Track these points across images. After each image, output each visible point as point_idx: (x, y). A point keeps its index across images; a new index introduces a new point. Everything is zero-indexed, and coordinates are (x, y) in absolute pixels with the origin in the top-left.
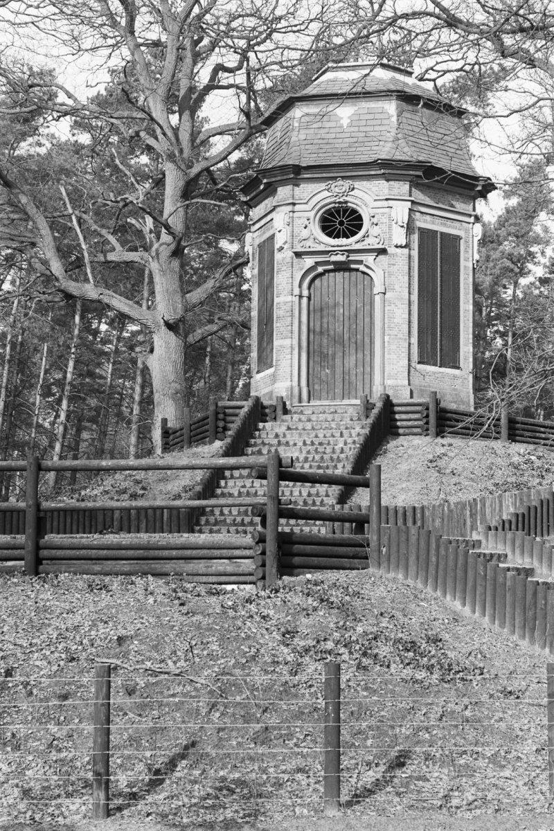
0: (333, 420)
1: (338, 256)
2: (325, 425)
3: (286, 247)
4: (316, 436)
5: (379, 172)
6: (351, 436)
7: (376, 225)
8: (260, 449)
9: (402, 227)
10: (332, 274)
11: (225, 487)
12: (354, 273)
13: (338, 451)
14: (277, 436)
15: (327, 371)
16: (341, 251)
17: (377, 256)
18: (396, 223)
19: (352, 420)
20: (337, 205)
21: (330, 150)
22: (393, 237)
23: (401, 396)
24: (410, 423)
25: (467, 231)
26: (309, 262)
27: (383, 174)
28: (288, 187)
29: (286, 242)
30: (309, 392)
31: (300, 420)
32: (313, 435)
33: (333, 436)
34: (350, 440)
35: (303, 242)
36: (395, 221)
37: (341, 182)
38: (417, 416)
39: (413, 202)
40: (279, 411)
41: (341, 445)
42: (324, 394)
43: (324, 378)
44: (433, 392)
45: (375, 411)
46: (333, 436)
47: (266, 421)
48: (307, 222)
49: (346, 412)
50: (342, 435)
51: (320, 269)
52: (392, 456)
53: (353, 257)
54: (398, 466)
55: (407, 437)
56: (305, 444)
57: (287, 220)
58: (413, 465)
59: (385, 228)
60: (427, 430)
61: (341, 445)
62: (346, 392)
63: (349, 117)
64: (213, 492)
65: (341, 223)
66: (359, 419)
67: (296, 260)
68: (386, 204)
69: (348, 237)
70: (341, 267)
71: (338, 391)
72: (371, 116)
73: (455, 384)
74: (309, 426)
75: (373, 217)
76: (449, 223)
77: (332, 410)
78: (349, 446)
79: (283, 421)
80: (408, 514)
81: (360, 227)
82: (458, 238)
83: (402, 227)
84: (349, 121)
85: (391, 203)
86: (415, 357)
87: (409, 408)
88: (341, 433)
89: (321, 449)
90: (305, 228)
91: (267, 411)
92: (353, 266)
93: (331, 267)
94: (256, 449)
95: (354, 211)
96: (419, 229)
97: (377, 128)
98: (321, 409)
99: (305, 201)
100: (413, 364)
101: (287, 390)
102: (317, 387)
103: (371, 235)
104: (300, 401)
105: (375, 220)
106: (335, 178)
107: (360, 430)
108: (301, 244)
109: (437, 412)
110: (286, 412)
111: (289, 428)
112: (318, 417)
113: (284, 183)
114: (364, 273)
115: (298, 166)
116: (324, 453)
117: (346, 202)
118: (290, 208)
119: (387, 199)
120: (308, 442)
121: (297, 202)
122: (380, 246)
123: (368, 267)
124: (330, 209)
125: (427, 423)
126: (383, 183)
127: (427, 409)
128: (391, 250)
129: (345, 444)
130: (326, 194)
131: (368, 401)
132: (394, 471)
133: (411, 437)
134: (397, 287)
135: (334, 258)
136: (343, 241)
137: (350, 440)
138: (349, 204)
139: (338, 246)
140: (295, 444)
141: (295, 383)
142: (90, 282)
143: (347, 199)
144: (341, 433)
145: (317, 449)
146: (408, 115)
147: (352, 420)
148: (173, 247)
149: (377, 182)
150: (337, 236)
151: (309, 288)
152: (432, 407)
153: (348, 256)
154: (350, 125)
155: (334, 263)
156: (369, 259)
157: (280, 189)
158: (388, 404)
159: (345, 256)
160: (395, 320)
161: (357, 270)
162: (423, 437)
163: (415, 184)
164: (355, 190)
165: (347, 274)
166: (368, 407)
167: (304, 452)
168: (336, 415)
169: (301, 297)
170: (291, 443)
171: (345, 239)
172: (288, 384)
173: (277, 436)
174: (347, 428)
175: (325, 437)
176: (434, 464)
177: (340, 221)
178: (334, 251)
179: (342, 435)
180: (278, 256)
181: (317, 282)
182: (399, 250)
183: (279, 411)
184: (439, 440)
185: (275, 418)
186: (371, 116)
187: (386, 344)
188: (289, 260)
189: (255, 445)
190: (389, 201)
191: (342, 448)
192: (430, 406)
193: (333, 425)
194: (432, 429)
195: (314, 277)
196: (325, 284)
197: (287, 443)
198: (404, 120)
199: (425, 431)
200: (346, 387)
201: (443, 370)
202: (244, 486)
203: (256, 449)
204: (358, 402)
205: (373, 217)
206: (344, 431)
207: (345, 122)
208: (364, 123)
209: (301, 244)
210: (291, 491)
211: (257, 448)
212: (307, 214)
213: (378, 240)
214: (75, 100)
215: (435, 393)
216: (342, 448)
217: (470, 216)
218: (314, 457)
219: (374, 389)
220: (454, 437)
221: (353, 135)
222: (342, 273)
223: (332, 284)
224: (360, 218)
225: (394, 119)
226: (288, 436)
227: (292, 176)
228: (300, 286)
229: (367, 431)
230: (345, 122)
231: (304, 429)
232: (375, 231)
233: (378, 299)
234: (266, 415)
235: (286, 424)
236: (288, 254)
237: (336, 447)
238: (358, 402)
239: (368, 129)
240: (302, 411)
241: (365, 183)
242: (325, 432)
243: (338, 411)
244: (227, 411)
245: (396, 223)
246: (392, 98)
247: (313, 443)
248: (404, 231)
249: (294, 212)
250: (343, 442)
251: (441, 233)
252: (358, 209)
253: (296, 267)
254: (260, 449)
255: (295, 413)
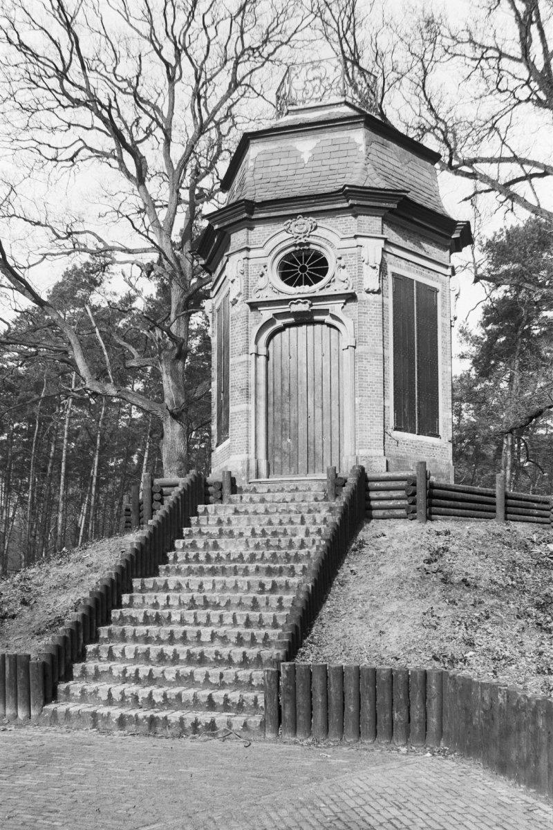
0: (293, 500)
1: (300, 304)
2: (282, 506)
3: (240, 299)
4: (270, 523)
5: (346, 205)
6: (314, 523)
7: (344, 267)
8: (194, 542)
9: (374, 268)
10: (293, 329)
11: (130, 605)
12: (318, 327)
13: (297, 544)
14: (220, 522)
15: (289, 440)
16: (303, 299)
17: (345, 304)
18: (367, 264)
19: (316, 500)
20: (298, 248)
21: (289, 187)
22: (365, 281)
23: (377, 469)
24: (391, 503)
25: (443, 284)
26: (267, 314)
27: (352, 206)
28: (242, 231)
29: (240, 294)
30: (268, 465)
31: (251, 500)
32: (266, 520)
33: (291, 522)
34: (313, 529)
35: (260, 292)
36: (366, 262)
37: (301, 220)
38: (399, 494)
39: (387, 242)
40: (226, 490)
41: (301, 535)
42: (286, 467)
43: (285, 449)
44: (421, 463)
45: (346, 490)
46: (291, 522)
47: (207, 502)
48: (264, 270)
49: (310, 490)
50: (303, 522)
51: (279, 323)
52: (371, 552)
53: (318, 306)
54: (381, 569)
55: (388, 521)
56: (253, 533)
57: (241, 267)
58: (403, 568)
59: (354, 271)
60: (414, 512)
61: (301, 535)
62: (311, 465)
63: (310, 151)
64: (109, 614)
65: (303, 269)
66: (326, 499)
67: (252, 314)
68: (354, 242)
69: (311, 285)
70: (304, 319)
71: (302, 463)
72: (336, 148)
73: (435, 453)
74: (261, 508)
75: (340, 258)
76: (425, 272)
77: (292, 487)
78: (312, 537)
79: (231, 502)
80: (413, 685)
81: (324, 272)
82: (435, 291)
83: (374, 268)
84: (311, 155)
85: (360, 241)
86: (391, 422)
87: (392, 484)
88: (302, 518)
89: (274, 542)
90: (262, 276)
91: (211, 489)
92: (316, 318)
93: (291, 320)
94: (188, 541)
95: (317, 255)
96: (394, 274)
97: (342, 160)
98: (278, 486)
99: (261, 246)
100: (389, 430)
101: (243, 464)
102: (277, 459)
103: (337, 279)
104: (258, 476)
105: (342, 262)
106: (294, 216)
107: (325, 516)
108: (257, 295)
109: (427, 489)
110: (234, 489)
111: (236, 512)
112: (273, 497)
113: (237, 226)
114: (330, 326)
115: (252, 202)
116: (279, 547)
117: (308, 244)
118: (244, 254)
119: (356, 237)
120: (258, 532)
121: (251, 247)
122: (349, 291)
123: (334, 317)
124: (290, 254)
125: (414, 503)
126: (350, 219)
127: (414, 485)
128: (362, 296)
129: (307, 533)
130: (285, 236)
131: (336, 475)
132: (377, 578)
133: (393, 522)
134: (368, 339)
135: (295, 308)
136: (305, 290)
137: (313, 529)
138: (312, 247)
139: (299, 293)
140: (241, 534)
141: (252, 456)
142: (110, 382)
143: (310, 240)
144: (302, 518)
145: (268, 541)
146: (378, 148)
147: (316, 500)
148: (176, 351)
149: (344, 219)
150: (299, 284)
151: (267, 346)
152: (420, 483)
153: (311, 305)
154: (312, 160)
155: (295, 314)
156: (336, 307)
157: (233, 236)
158: (362, 477)
159: (307, 305)
160: (369, 379)
161: (322, 322)
162: (407, 521)
163: (391, 219)
164: (318, 229)
165: (310, 328)
166: (337, 483)
167: (251, 545)
168: (297, 494)
169: (257, 355)
170: (236, 533)
171: (307, 286)
172: (244, 456)
173: (220, 522)
174: (310, 512)
175: (281, 523)
176: (435, 566)
177: (303, 266)
178: (295, 299)
179: (303, 522)
180: (233, 311)
181: (278, 337)
182: (371, 296)
183: (226, 490)
184: (430, 525)
185: (221, 498)
186: (336, 148)
187: (357, 407)
188: (244, 314)
189: (190, 535)
190: (359, 239)
191: (302, 541)
192: (418, 481)
193: (293, 507)
194: (421, 510)
195: (272, 331)
196: (286, 341)
197: (231, 532)
198: (373, 152)
199: (411, 514)
200: (311, 459)
201: (421, 438)
202: (156, 605)
203: (188, 541)
204: (324, 476)
205: (340, 258)
206: (306, 516)
207: (306, 157)
208: (328, 155)
209: (257, 295)
210: (221, 617)
211: (190, 541)
212: (263, 261)
213: (345, 285)
214: (105, 243)
215: (423, 464)
216: (302, 541)
217: (447, 267)
218: (263, 554)
219: (344, 461)
220: (446, 520)
221: (315, 169)
222: (304, 327)
223: (294, 340)
224: (324, 262)
225: (363, 148)
226: (234, 522)
227: (245, 215)
228: (256, 342)
229: (335, 519)
230: (306, 157)
231: (255, 513)
232: (343, 274)
233: (347, 355)
234: (208, 494)
235: (233, 506)
236: (242, 308)
237: (294, 539)
238: (324, 476)
239: (330, 162)
240: (255, 489)
241: (330, 220)
242: (281, 517)
243: (300, 488)
244: (164, 489)
245: (367, 264)
246: (359, 125)
247: (264, 533)
248: (376, 273)
249: (248, 259)
250: (304, 531)
251: (417, 282)
252: (323, 251)
253: (252, 321)
254: (194, 542)
255: (247, 491)
